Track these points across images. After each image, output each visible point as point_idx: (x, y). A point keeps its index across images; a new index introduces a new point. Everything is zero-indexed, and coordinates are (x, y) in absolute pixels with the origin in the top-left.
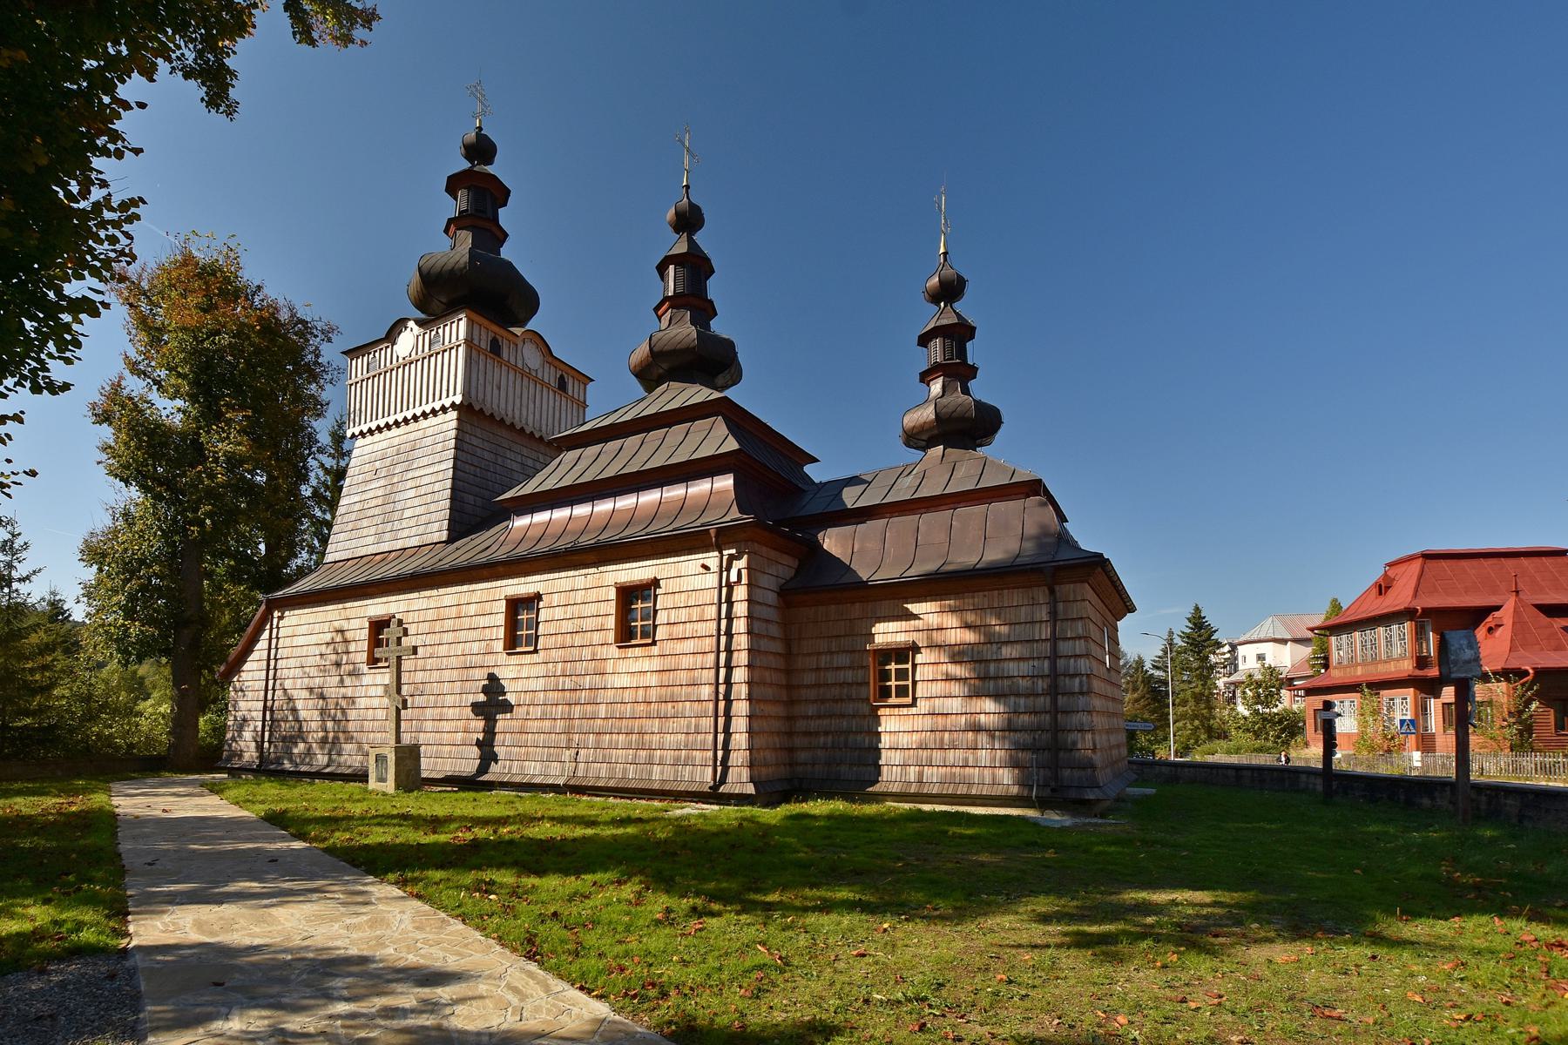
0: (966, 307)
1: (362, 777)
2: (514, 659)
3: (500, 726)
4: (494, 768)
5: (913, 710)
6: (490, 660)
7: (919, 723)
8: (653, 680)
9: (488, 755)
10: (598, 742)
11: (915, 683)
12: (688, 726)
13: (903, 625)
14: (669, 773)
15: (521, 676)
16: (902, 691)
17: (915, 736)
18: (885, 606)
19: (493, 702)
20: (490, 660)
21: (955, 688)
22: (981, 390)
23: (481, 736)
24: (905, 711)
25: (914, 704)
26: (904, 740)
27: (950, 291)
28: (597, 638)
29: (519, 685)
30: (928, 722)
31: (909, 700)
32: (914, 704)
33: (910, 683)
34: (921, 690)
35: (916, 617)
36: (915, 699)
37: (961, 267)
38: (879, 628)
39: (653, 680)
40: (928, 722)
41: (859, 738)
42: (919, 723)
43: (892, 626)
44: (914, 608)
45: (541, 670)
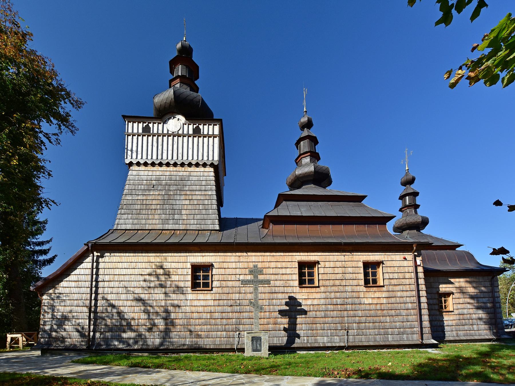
0: (414, 187)
1: (242, 350)
2: (304, 290)
3: (299, 320)
4: (297, 340)
5: (453, 313)
6: (290, 290)
7: (455, 317)
8: (384, 301)
9: (292, 332)
10: (359, 327)
11: (212, 281)
12: (403, 319)
13: (450, 286)
14: (397, 337)
15: (306, 297)
16: (206, 285)
17: (454, 322)
18: (441, 279)
19: (293, 309)
20: (290, 290)
21: (469, 306)
22: (421, 212)
23: (286, 326)
24: (209, 292)
25: (212, 290)
26: (450, 323)
27: (410, 182)
28: (355, 282)
29: (309, 302)
30: (458, 317)
31: (210, 289)
32: (212, 290)
33: (210, 281)
34: (215, 284)
35: (452, 283)
36: (212, 288)
37: (412, 174)
38: (441, 286)
39: (384, 301)
40: (458, 317)
41: (436, 323)
42: (455, 317)
43: (444, 286)
44: (452, 280)
45: (323, 295)
